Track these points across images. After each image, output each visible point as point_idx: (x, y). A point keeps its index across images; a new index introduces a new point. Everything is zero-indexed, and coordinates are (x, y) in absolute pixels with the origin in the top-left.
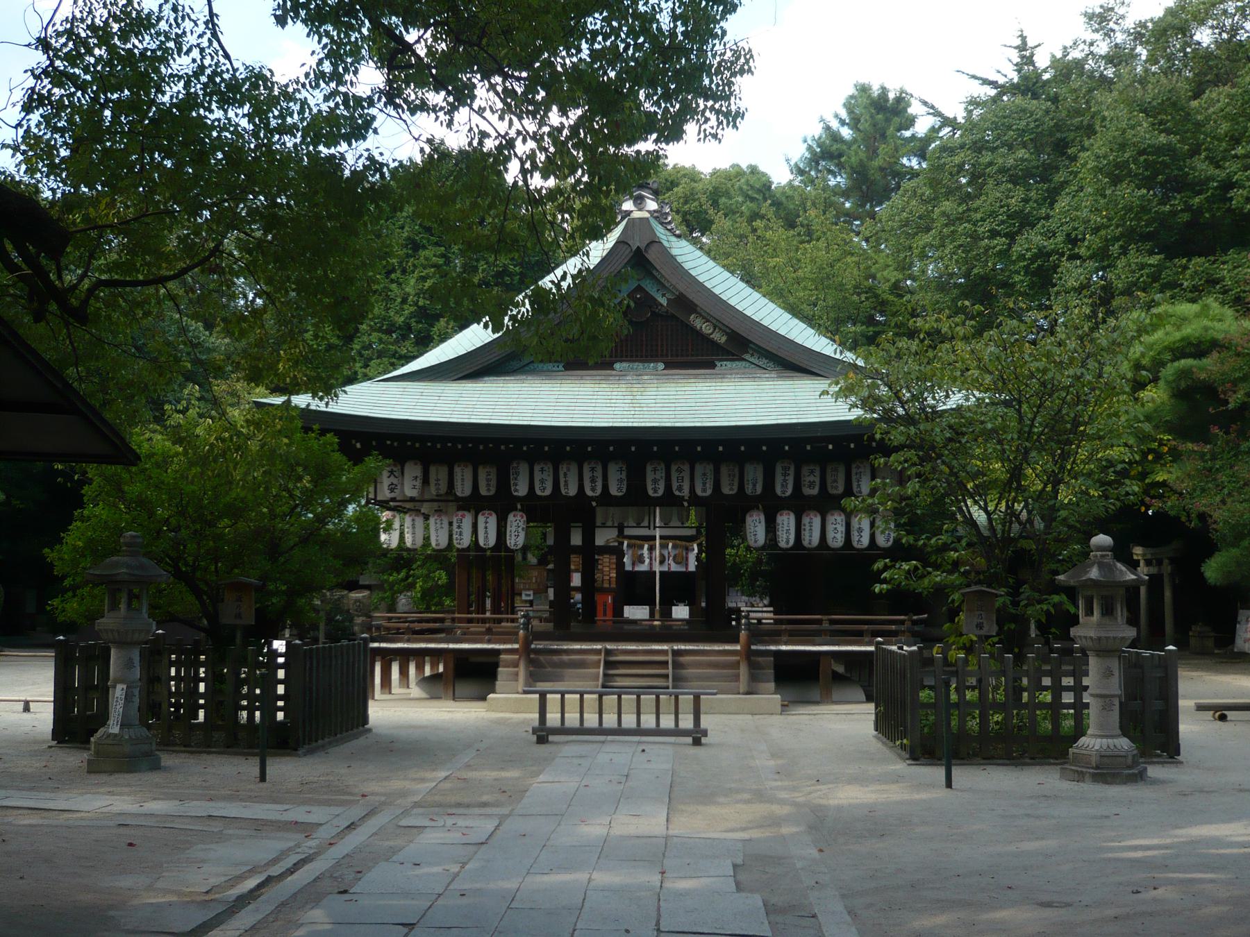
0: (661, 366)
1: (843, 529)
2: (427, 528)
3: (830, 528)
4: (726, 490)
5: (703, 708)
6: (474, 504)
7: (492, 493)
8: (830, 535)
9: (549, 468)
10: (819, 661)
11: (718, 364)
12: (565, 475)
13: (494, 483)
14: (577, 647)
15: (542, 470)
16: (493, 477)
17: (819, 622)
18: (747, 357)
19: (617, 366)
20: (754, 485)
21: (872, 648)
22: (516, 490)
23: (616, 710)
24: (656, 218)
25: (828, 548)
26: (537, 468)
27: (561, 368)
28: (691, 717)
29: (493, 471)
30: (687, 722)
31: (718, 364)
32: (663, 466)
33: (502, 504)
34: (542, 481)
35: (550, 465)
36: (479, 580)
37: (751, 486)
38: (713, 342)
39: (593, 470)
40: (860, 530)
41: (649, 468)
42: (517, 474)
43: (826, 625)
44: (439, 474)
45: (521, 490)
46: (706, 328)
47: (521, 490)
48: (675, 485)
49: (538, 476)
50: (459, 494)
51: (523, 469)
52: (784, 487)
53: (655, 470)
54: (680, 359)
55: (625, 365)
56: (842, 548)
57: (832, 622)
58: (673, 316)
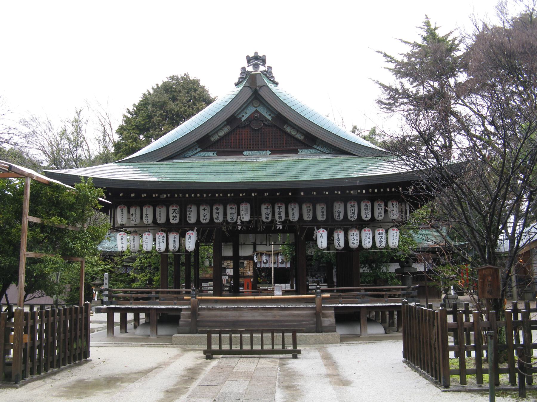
0: (269, 152)
1: (358, 238)
2: (154, 240)
3: (350, 238)
4: (306, 218)
5: (298, 341)
6: (167, 228)
7: (324, 219)
8: (351, 242)
9: (208, 208)
10: (359, 313)
11: (300, 151)
12: (293, 210)
13: (325, 213)
14: (302, 306)
15: (205, 209)
16: (325, 210)
17: (359, 290)
18: (315, 147)
19: (245, 153)
20: (339, 214)
21: (400, 304)
22: (190, 220)
23: (218, 342)
24: (265, 75)
25: (363, 249)
26: (201, 208)
27: (215, 154)
28: (239, 346)
29: (325, 207)
30: (291, 348)
31: (300, 151)
32: (271, 206)
33: (182, 229)
34: (204, 215)
35: (209, 207)
36: (176, 270)
37: (337, 215)
38: (297, 139)
39: (279, 208)
40: (339, 239)
41: (263, 207)
42: (191, 211)
43: (363, 292)
44: (148, 211)
45: (192, 219)
46: (293, 132)
47: (192, 219)
48: (215, 216)
49: (202, 212)
50: (264, 220)
51: (194, 209)
52: (339, 215)
53: (232, 209)
54: (285, 148)
55: (250, 152)
56: (371, 248)
57: (366, 290)
58: (275, 126)
